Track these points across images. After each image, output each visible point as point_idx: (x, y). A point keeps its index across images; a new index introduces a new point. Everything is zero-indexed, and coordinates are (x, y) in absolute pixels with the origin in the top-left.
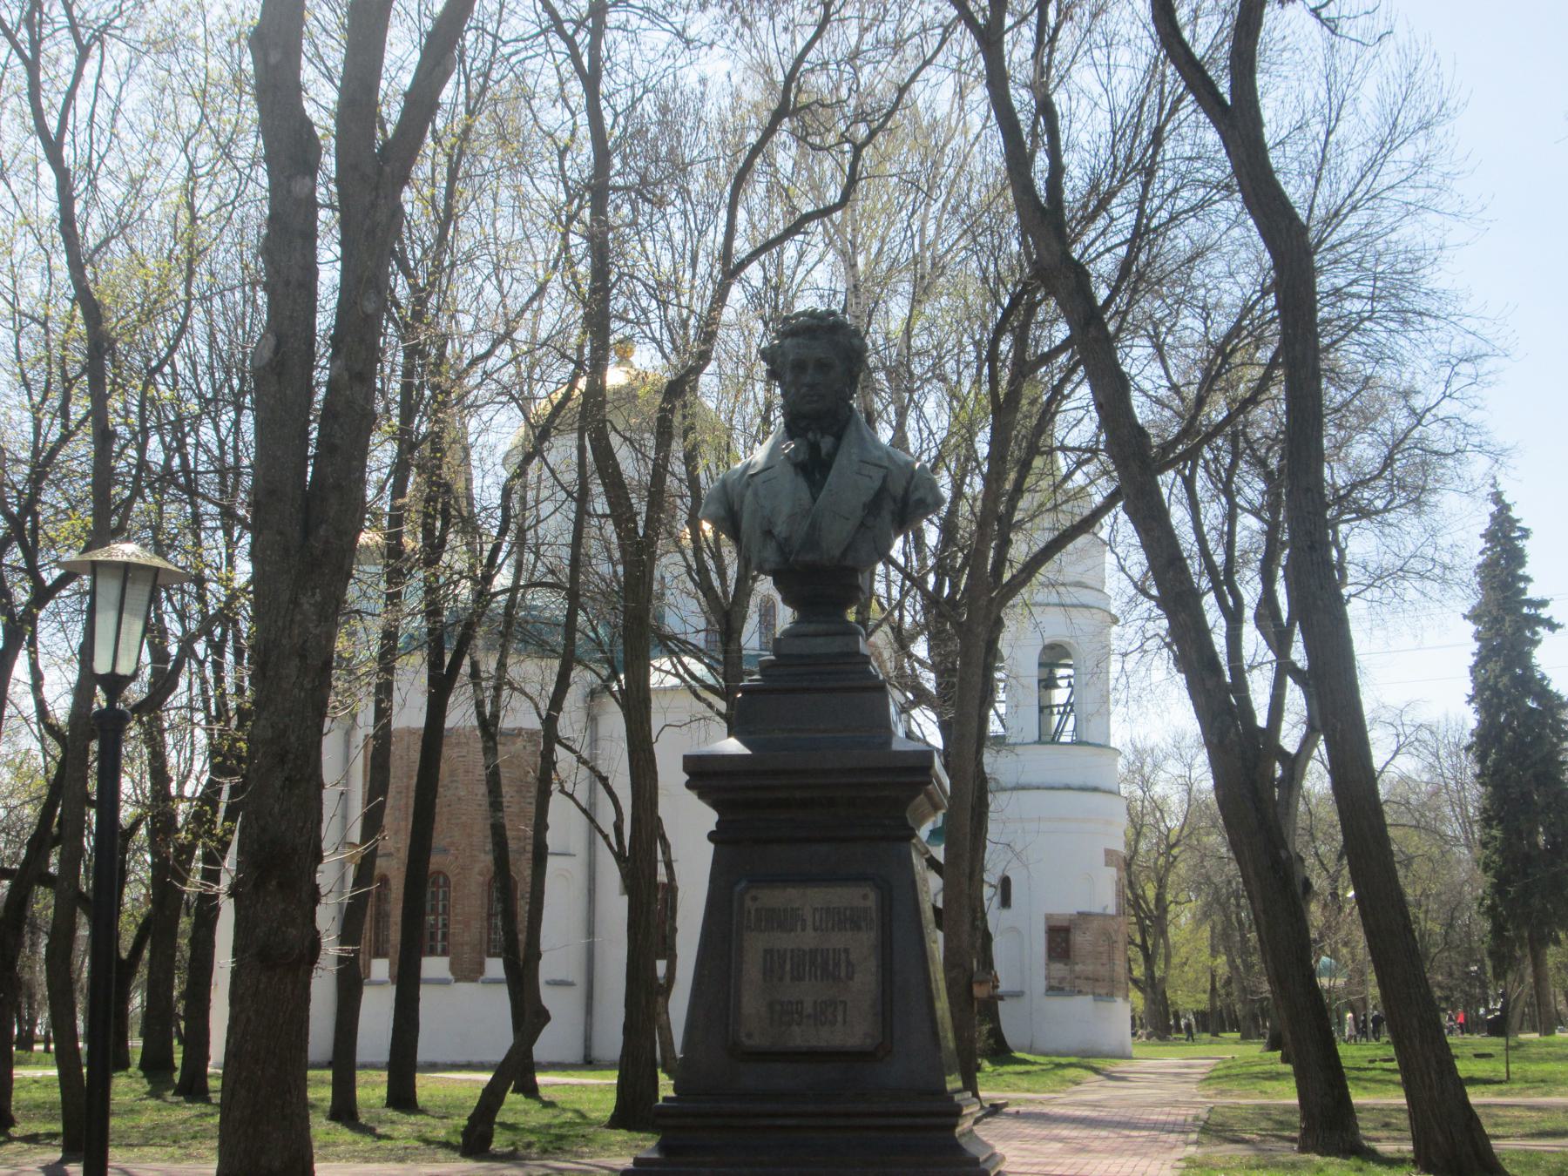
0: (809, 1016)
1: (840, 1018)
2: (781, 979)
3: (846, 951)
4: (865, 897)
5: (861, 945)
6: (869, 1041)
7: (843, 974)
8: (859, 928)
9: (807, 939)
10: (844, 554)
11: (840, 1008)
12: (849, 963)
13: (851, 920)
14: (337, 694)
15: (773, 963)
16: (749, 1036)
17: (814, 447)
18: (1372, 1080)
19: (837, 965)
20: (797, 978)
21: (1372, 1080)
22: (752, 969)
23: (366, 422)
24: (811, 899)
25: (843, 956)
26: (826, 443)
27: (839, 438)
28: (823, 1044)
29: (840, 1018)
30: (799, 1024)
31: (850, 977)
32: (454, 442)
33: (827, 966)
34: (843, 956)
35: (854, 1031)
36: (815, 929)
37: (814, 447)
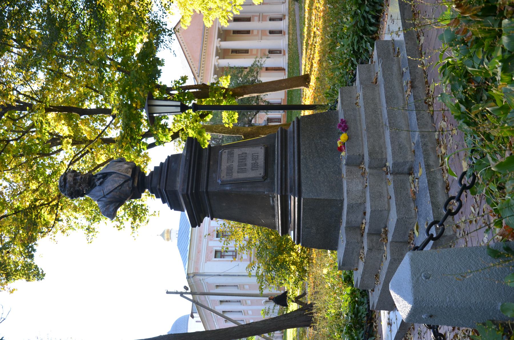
2: (245, 169)
4: (225, 152)
6: (263, 148)
9: (235, 165)
12: (243, 154)
13: (231, 154)
15: (241, 170)
16: (260, 174)
19: (242, 157)
22: (242, 176)
24: (224, 165)
31: (246, 153)
33: (243, 158)
35: (260, 151)
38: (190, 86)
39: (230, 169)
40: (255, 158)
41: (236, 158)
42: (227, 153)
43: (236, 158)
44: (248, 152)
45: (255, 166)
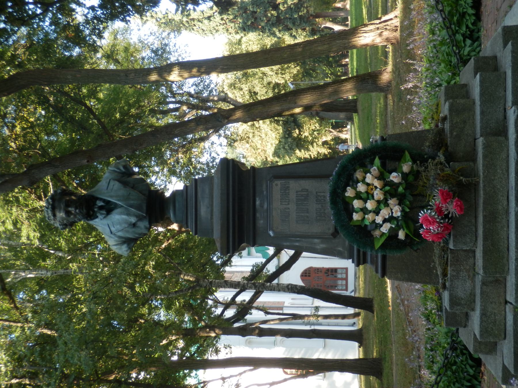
1: (322, 194)
2: (307, 217)
3: (297, 192)
8: (288, 187)
10: (144, 195)
11: (319, 194)
12: (302, 191)
13: (285, 190)
17: (101, 208)
24: (277, 205)
25: (299, 193)
26: (100, 203)
27: (98, 199)
29: (322, 194)
34: (299, 193)
36: (289, 204)
37: (101, 208)
41: (293, 196)
42: (279, 186)
43: (293, 196)
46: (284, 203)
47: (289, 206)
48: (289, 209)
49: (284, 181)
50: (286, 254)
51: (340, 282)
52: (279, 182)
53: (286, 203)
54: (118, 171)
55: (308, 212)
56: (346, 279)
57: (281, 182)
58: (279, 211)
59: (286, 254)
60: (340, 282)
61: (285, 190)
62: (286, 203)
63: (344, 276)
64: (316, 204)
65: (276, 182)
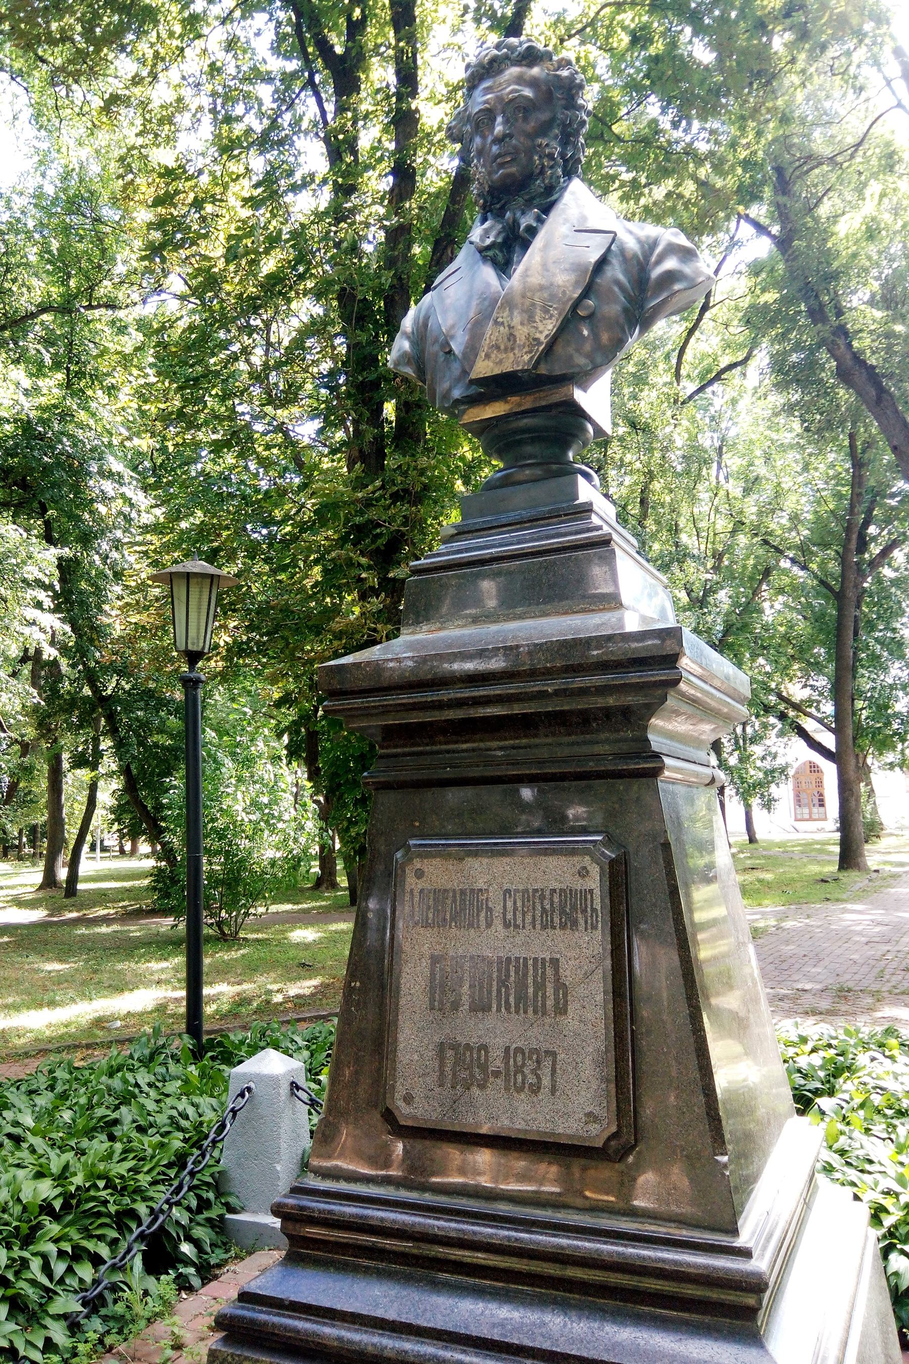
0: (497, 1074)
2: (456, 1006)
3: (555, 962)
4: (583, 873)
5: (582, 952)
7: (550, 1003)
9: (492, 942)
11: (547, 1063)
12: (560, 986)
13: (564, 911)
14: (66, 721)
18: (548, 673)
19: (540, 986)
20: (480, 1007)
21: (548, 673)
22: (413, 981)
23: (507, 1281)
24: (497, 875)
25: (549, 972)
28: (520, 1125)
29: (546, 1081)
30: (482, 1087)
31: (561, 1010)
32: (844, 95)
34: (549, 972)
36: (507, 925)
38: (819, 744)
39: (462, 908)
40: (526, 1069)
41: (536, 944)
42: (579, 885)
43: (536, 944)
44: (571, 1021)
45: (463, 1065)
46: (510, 904)
47: (498, 924)
48: (489, 925)
49: (598, 905)
50: (829, 740)
51: (806, 810)
52: (595, 882)
53: (510, 916)
54: (653, 259)
55: (473, 1009)
56: (810, 819)
57: (597, 892)
58: (481, 884)
59: (829, 740)
60: (806, 810)
61: (564, 911)
62: (510, 916)
63: (815, 816)
64: (507, 1049)
65: (595, 870)
